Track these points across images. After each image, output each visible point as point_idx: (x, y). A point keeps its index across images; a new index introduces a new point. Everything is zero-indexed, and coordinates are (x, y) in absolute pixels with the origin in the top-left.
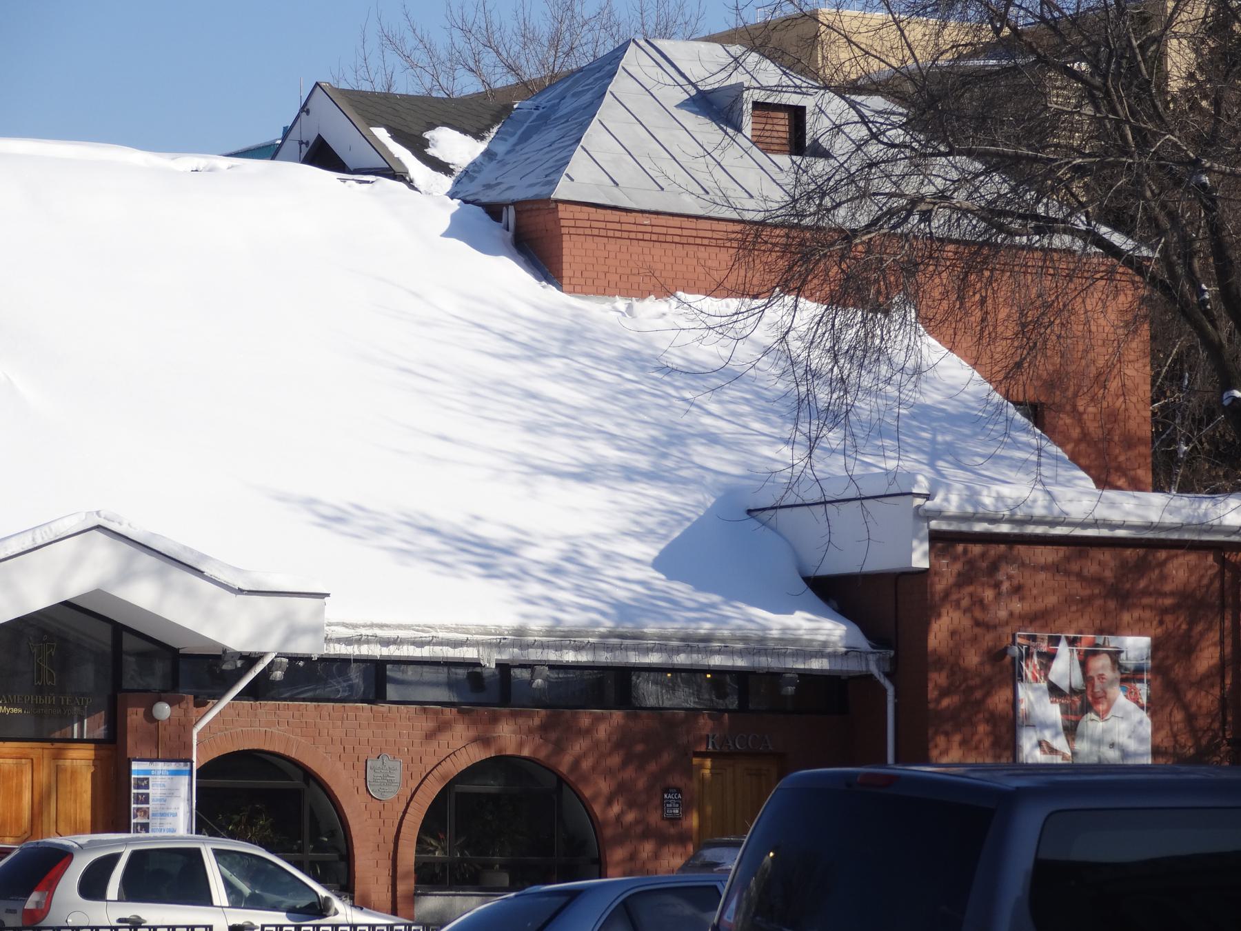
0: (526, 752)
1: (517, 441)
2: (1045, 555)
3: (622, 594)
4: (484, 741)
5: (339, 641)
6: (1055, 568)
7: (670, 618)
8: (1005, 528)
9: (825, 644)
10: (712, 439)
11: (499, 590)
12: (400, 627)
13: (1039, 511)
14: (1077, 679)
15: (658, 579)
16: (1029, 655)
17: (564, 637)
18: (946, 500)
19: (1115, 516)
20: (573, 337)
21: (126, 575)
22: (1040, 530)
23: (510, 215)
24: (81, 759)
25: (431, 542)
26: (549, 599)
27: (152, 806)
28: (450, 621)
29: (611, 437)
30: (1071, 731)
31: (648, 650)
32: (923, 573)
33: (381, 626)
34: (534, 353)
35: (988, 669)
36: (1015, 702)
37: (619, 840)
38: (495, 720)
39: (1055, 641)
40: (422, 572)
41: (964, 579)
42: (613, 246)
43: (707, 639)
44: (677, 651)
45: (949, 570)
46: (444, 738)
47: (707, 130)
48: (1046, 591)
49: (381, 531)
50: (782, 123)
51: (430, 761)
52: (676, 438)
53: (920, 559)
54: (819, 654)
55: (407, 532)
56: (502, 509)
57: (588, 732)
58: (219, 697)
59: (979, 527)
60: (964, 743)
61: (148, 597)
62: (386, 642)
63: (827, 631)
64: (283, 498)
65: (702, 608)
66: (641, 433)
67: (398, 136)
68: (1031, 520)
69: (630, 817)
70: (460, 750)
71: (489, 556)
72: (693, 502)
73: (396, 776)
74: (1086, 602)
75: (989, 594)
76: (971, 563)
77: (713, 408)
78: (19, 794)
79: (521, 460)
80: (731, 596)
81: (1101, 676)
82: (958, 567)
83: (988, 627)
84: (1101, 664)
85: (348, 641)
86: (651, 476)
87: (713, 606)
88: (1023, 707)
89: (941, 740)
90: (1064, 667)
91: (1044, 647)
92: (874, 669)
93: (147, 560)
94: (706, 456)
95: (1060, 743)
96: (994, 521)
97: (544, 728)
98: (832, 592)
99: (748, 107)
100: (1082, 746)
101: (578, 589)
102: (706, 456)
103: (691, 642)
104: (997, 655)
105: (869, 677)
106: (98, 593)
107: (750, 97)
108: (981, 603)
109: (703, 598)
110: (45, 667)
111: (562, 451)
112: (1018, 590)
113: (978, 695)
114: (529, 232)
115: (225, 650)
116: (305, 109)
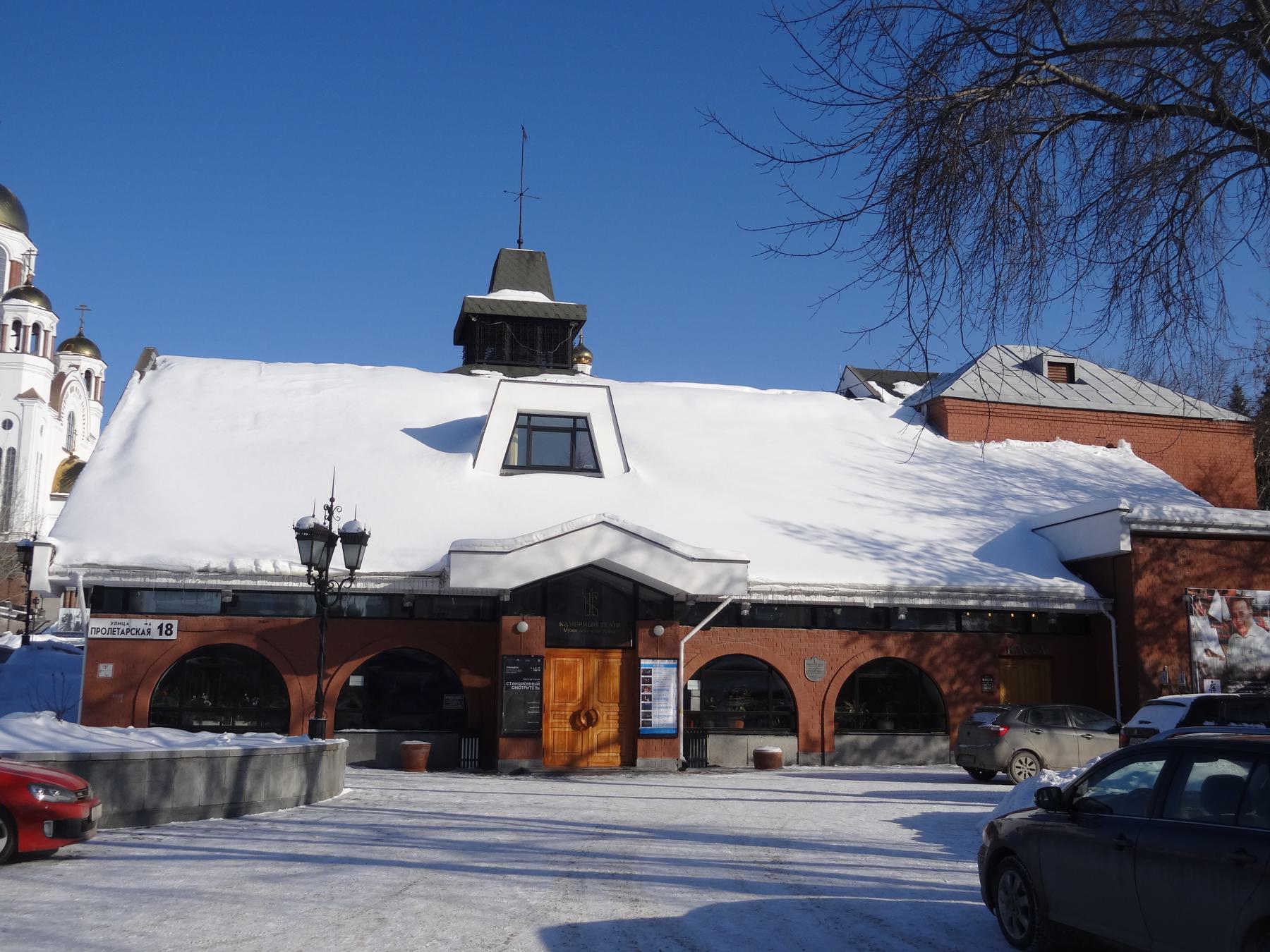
0: (902, 655)
1: (908, 498)
2: (1205, 544)
3: (953, 568)
4: (877, 647)
5: (779, 593)
6: (1211, 551)
7: (979, 580)
8: (1178, 529)
9: (1073, 595)
10: (1017, 497)
11: (883, 565)
12: (815, 585)
13: (1198, 519)
14: (1227, 613)
15: (976, 561)
16: (1196, 600)
17: (918, 592)
18: (1141, 511)
19: (1247, 522)
20: (947, 456)
21: (626, 549)
22: (1199, 530)
23: (925, 408)
24: (615, 659)
25: (848, 542)
26: (908, 570)
27: (654, 685)
28: (845, 581)
29: (961, 497)
30: (1224, 642)
31: (966, 599)
32: (1128, 554)
33: (804, 585)
34: (927, 461)
35: (1173, 607)
36: (1189, 626)
37: (956, 704)
38: (885, 636)
39: (1212, 593)
40: (839, 557)
41: (1157, 556)
42: (973, 418)
43: (1003, 592)
44: (984, 599)
45: (1146, 552)
46: (852, 647)
47: (1027, 375)
48: (1206, 562)
49: (820, 537)
50: (1063, 372)
51: (843, 660)
52: (997, 496)
53: (1126, 545)
54: (1071, 601)
55: (835, 538)
56: (890, 526)
57: (939, 643)
58: (695, 625)
59: (1162, 528)
60: (1161, 649)
61: (638, 562)
62: (808, 594)
63: (1078, 588)
64: (770, 522)
65: (1000, 575)
66: (977, 495)
67: (879, 384)
68: (1194, 525)
69: (967, 689)
70: (863, 652)
71: (878, 549)
72: (1000, 525)
73: (823, 669)
74: (1230, 570)
75: (1171, 566)
76: (1159, 548)
77: (1020, 485)
78: (575, 680)
79: (909, 506)
80: (1017, 569)
81: (1241, 613)
82: (1151, 550)
83: (1172, 583)
84: (1242, 605)
85: (785, 593)
86: (981, 513)
87: (1006, 574)
88: (1194, 630)
89: (1146, 648)
90: (1218, 606)
91: (1206, 596)
92: (1102, 609)
93: (637, 542)
94: (1010, 504)
95: (1218, 650)
96: (1168, 524)
97: (912, 641)
98: (1076, 568)
99: (1045, 366)
100: (1235, 651)
101: (928, 566)
102: (1010, 504)
103: (992, 594)
104: (1178, 600)
105: (1100, 615)
106: (603, 560)
107: (1046, 360)
108: (1166, 570)
109: (1000, 570)
110: (592, 606)
111: (933, 502)
112: (1189, 563)
113: (1168, 622)
114: (932, 413)
115: (687, 595)
116: (842, 379)
